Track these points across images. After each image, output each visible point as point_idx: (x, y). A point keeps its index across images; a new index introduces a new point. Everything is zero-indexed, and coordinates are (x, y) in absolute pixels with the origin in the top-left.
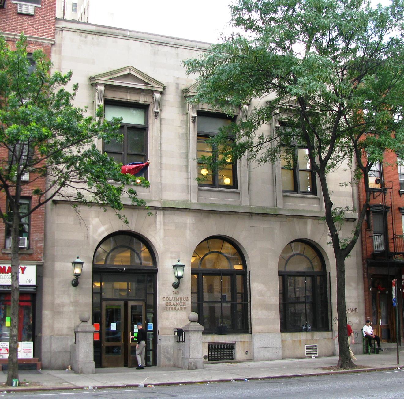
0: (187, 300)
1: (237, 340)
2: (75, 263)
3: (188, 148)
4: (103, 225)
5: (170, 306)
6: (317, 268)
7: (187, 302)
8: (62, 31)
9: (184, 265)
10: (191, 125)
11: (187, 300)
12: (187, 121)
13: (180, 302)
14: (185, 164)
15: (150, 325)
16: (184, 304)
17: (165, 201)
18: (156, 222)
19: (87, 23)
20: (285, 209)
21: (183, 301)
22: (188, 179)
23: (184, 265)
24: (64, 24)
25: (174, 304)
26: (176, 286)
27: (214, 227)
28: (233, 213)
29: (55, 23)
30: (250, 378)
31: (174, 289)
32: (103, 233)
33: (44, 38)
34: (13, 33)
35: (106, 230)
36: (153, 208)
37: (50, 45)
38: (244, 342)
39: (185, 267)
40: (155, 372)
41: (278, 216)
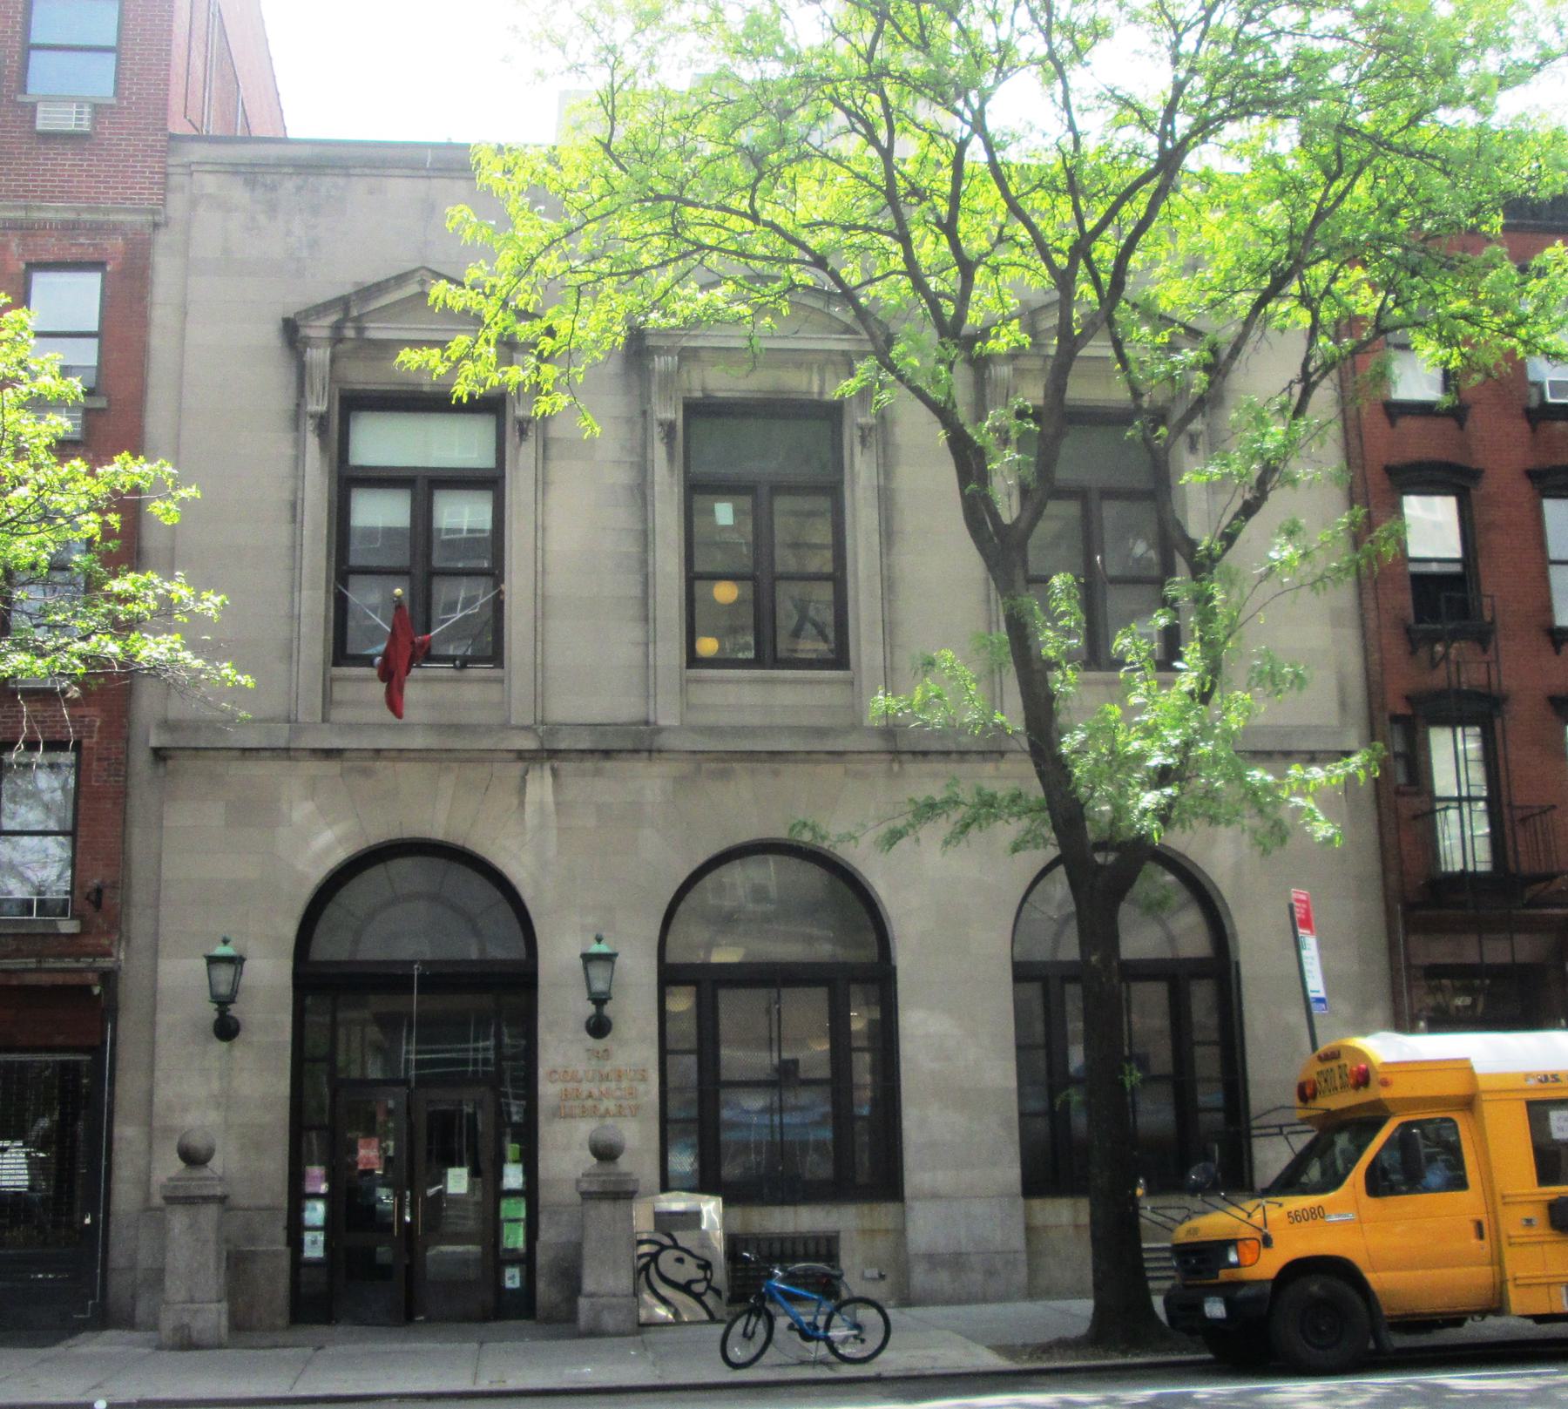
0: (644, 1079)
1: (840, 1225)
2: (213, 961)
3: (645, 538)
4: (329, 825)
5: (576, 1103)
6: (869, 954)
7: (641, 1087)
8: (191, 174)
9: (615, 955)
10: (659, 452)
11: (644, 1079)
12: (645, 445)
13: (613, 1085)
14: (636, 591)
15: (513, 1177)
16: (632, 1094)
17: (554, 729)
18: (522, 804)
19: (248, 140)
20: (694, 729)
21: (625, 1084)
22: (647, 645)
23: (615, 955)
24: (199, 152)
25: (590, 1096)
26: (599, 1027)
27: (749, 808)
28: (822, 756)
29: (167, 152)
30: (1544, 1309)
31: (591, 1042)
32: (328, 850)
33: (128, 205)
34: (22, 202)
35: (340, 841)
36: (512, 755)
37: (148, 230)
38: (873, 1232)
39: (618, 960)
40: (396, 1346)
41: (347, 754)
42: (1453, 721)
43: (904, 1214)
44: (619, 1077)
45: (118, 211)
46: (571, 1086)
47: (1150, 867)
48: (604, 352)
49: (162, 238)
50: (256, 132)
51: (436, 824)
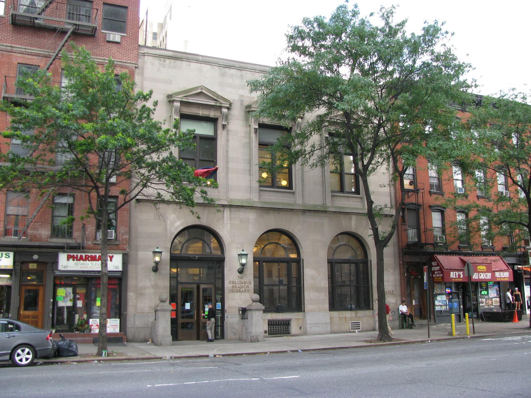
0: (250, 284)
1: (292, 318)
3: (250, 155)
4: (179, 220)
7: (250, 286)
14: (248, 168)
16: (248, 287)
19: (166, 50)
21: (246, 285)
24: (146, 50)
29: (138, 49)
31: (239, 274)
32: (179, 226)
37: (134, 68)
42: (66, 285)
43: (304, 316)
44: (245, 283)
45: (126, 63)
46: (234, 285)
47: (67, 329)
48: (409, 145)
49: (137, 71)
50: (167, 48)
51: (204, 222)
